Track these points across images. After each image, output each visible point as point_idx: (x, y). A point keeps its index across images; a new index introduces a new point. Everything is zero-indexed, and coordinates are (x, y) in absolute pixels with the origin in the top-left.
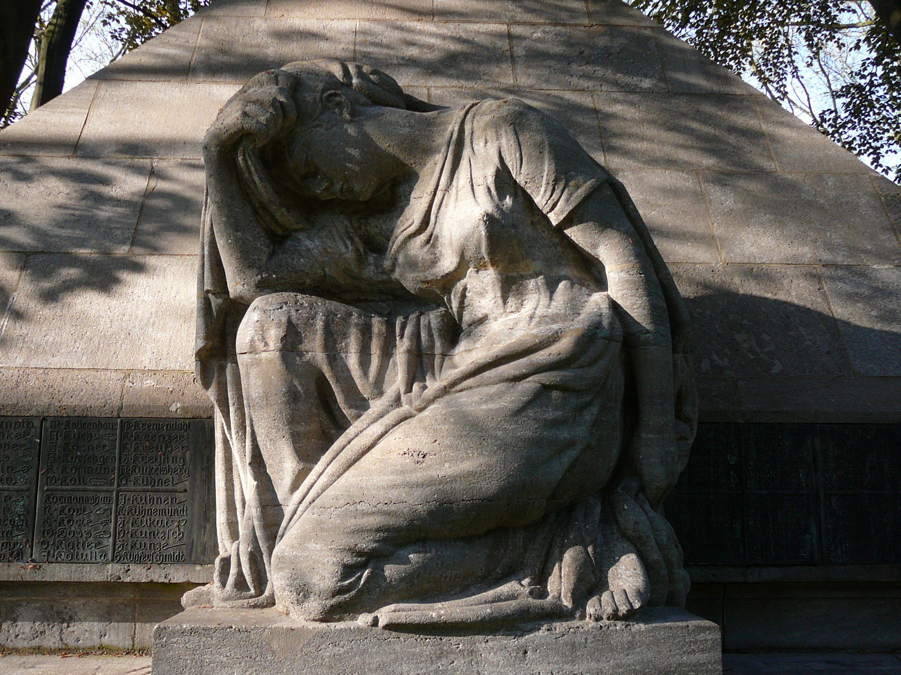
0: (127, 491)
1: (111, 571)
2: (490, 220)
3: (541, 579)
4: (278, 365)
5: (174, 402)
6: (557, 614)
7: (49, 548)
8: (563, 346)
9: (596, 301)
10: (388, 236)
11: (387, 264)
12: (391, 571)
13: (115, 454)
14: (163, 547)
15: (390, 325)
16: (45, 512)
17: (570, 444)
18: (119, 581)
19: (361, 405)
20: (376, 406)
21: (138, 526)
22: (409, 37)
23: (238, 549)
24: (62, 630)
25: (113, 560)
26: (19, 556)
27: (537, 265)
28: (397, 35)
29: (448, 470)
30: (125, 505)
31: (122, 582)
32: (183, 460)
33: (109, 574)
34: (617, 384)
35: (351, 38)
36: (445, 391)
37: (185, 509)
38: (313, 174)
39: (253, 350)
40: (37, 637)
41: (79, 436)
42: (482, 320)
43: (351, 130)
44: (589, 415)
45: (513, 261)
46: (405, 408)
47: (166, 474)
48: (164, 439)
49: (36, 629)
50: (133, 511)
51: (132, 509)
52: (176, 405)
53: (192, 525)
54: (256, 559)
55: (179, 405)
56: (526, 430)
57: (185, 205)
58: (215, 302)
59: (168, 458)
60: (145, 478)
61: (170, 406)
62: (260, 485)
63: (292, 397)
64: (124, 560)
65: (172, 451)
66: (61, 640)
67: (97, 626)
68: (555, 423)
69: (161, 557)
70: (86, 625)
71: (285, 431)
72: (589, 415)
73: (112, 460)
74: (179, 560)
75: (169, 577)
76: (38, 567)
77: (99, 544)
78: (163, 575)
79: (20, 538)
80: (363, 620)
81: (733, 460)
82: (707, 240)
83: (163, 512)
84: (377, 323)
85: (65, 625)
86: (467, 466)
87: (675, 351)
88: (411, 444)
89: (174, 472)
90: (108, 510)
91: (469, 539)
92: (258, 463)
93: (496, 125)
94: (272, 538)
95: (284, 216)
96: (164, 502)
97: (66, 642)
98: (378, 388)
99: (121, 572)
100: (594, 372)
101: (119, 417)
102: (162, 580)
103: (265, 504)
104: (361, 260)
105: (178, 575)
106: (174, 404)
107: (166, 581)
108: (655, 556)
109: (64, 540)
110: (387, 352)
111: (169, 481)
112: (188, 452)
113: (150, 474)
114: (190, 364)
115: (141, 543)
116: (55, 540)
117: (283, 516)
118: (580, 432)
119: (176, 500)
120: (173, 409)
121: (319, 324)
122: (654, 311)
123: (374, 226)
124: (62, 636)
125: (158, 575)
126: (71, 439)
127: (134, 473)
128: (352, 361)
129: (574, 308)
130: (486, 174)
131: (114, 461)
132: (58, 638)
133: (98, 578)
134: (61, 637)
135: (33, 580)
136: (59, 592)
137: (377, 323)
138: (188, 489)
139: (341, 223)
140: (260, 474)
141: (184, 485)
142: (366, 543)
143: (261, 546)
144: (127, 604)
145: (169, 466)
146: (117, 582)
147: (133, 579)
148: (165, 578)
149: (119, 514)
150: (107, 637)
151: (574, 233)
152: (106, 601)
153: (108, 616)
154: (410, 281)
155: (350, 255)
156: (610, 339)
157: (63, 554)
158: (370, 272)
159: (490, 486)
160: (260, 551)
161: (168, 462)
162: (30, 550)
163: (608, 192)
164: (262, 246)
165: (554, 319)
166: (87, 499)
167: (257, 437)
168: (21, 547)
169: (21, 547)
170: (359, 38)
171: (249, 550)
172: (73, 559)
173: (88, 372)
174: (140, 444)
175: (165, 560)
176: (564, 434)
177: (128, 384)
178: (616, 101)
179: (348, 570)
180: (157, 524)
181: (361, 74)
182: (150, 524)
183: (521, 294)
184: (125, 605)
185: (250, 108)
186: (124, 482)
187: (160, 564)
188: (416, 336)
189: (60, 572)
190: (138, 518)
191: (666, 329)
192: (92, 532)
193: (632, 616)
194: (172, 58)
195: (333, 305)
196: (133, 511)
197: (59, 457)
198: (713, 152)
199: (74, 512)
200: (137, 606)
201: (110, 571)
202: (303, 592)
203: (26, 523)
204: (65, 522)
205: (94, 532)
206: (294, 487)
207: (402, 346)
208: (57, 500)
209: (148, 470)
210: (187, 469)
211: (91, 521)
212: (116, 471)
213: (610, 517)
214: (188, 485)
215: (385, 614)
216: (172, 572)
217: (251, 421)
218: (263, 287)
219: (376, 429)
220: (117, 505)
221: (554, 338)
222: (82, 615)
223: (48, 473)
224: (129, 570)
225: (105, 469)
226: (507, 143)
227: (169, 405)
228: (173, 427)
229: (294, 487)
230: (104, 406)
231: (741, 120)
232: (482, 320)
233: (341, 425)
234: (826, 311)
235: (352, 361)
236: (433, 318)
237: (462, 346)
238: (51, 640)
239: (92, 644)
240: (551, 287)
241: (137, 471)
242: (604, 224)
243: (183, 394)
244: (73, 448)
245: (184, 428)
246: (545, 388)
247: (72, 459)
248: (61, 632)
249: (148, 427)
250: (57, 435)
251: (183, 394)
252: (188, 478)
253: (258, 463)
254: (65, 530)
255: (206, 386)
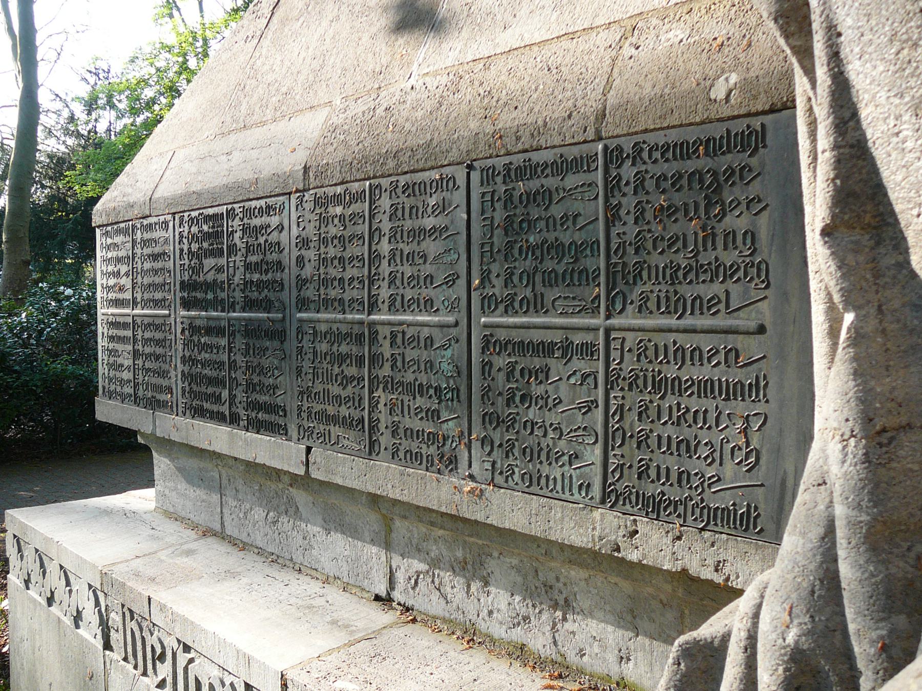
0: (625, 330)
5: (723, 72)
7: (495, 453)
13: (598, 234)
14: (709, 486)
16: (483, 374)
18: (616, 554)
21: (652, 421)
23: (756, 616)
24: (554, 625)
25: (603, 502)
30: (623, 366)
31: (623, 559)
32: (753, 243)
33: (597, 533)
37: (762, 384)
40: (519, 624)
41: (528, 198)
47: (712, 281)
48: (701, 181)
49: (515, 609)
50: (640, 382)
51: (637, 377)
52: (727, 79)
53: (781, 430)
55: (734, 78)
59: (714, 235)
60: (662, 295)
61: (712, 86)
62: (871, 325)
64: (624, 504)
65: (724, 215)
66: (555, 643)
67: (613, 635)
69: (706, 511)
70: (593, 627)
73: (592, 250)
75: (727, 570)
76: (478, 492)
77: (577, 457)
78: (710, 562)
83: (706, 388)
85: (559, 614)
89: (731, 276)
90: (589, 375)
96: (709, 361)
97: (562, 650)
99: (621, 534)
101: (600, 139)
102: (707, 574)
103: (893, 421)
106: (723, 77)
107: (719, 579)
109: (517, 440)
111: (719, 302)
112: (765, 214)
113: (673, 284)
115: (658, 467)
116: (502, 437)
117: (696, 629)
119: (737, 357)
120: (719, 92)
124: (556, 635)
126: (515, 207)
127: (639, 283)
131: (596, 253)
132: (549, 635)
133: (578, 538)
134: (554, 637)
135: (473, 518)
136: (539, 546)
138: (769, 327)
140: (877, 275)
141: (758, 312)
143: (852, 627)
144: (665, 601)
145: (717, 259)
146: (611, 556)
147: (644, 556)
148: (717, 570)
149: (612, 388)
150: (631, 664)
157: (516, 470)
160: (848, 656)
161: (715, 249)
162: (467, 454)
166: (546, 349)
167: (861, 106)
168: (454, 445)
169: (454, 445)
171: (791, 638)
173: (554, 47)
174: (648, 202)
177: (628, 51)
180: (695, 422)
182: (679, 417)
184: (661, 601)
186: (619, 307)
187: (702, 529)
190: (651, 402)
192: (563, 427)
196: (640, 382)
197: (499, 251)
199: (530, 377)
200: (686, 612)
201: (598, 526)
203: (458, 396)
204: (517, 399)
205: (567, 427)
208: (500, 349)
209: (668, 272)
210: (763, 266)
211: (561, 402)
212: (602, 279)
214: (767, 314)
216: (730, 559)
217: (833, 33)
220: (607, 364)
222: (584, 602)
223: (484, 288)
224: (637, 532)
225: (581, 272)
227: (708, 83)
228: (721, 147)
230: (570, 116)
239: (606, 672)
241: (645, 274)
243: (749, 45)
244: (521, 228)
245: (749, 146)
247: (520, 253)
248: (553, 628)
249: (662, 155)
250: (492, 200)
251: (749, 45)
252: (767, 292)
254: (518, 418)
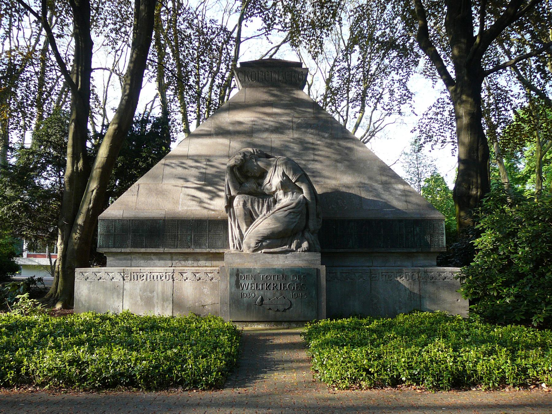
1: (208, 250)
2: (281, 182)
3: (290, 246)
4: (242, 209)
6: (292, 251)
8: (293, 205)
9: (301, 195)
10: (263, 183)
11: (262, 188)
12: (264, 243)
15: (263, 201)
17: (295, 222)
19: (258, 216)
20: (261, 216)
22: (265, 122)
26: (189, 247)
27: (290, 190)
28: (263, 122)
29: (273, 226)
34: (305, 211)
35: (251, 123)
36: (273, 213)
38: (248, 171)
39: (237, 206)
42: (281, 200)
43: (255, 163)
44: (299, 217)
45: (286, 189)
46: (266, 216)
54: (239, 244)
56: (287, 219)
57: (57, 37)
58: (228, 196)
63: (245, 214)
67: (204, 262)
68: (292, 218)
71: (244, 221)
72: (299, 217)
74: (221, 248)
79: (189, 244)
80: (259, 252)
81: (334, 227)
82: (335, 179)
84: (261, 200)
86: (277, 226)
87: (316, 205)
88: (267, 222)
91: (277, 239)
92: (239, 227)
93: (282, 164)
94: (242, 241)
95: (242, 180)
98: (261, 212)
100: (299, 209)
104: (257, 188)
105: (221, 251)
108: (311, 242)
110: (263, 206)
114: (224, 209)
118: (297, 220)
121: (250, 201)
122: (311, 198)
123: (260, 181)
125: (217, 251)
128: (256, 208)
129: (297, 198)
130: (280, 173)
137: (261, 200)
139: (253, 181)
142: (260, 239)
151: (297, 183)
152: (206, 257)
153: (206, 260)
154: (267, 192)
155: (255, 187)
156: (302, 203)
158: (259, 190)
159: (281, 229)
163: (303, 176)
164: (238, 186)
165: (293, 200)
170: (253, 123)
172: (200, 248)
175: (218, 248)
176: (294, 220)
178: (318, 140)
179: (257, 243)
181: (257, 152)
183: (287, 195)
185: (237, 161)
188: (268, 203)
189: (198, 250)
191: (315, 201)
193: (305, 251)
194: (207, 131)
195: (252, 197)
198: (340, 154)
202: (249, 248)
206: (246, 231)
207: (266, 205)
213: (303, 235)
215: (263, 251)
218: (238, 194)
219: (261, 220)
221: (292, 204)
226: (284, 167)
229: (246, 231)
231: (350, 145)
232: (281, 200)
233: (254, 220)
234: (359, 194)
235: (256, 208)
236: (271, 199)
237: (277, 204)
238: (195, 264)
240: (293, 193)
242: (302, 182)
246: (290, 212)
253: (239, 227)
255: (227, 213)
